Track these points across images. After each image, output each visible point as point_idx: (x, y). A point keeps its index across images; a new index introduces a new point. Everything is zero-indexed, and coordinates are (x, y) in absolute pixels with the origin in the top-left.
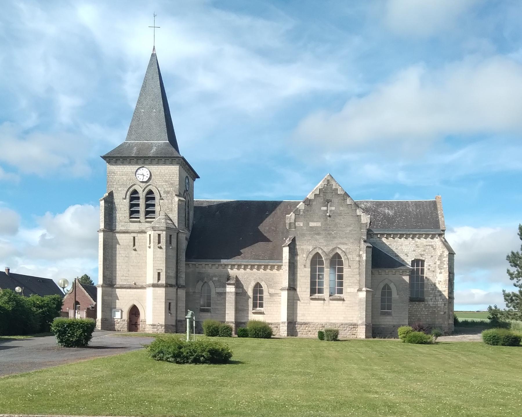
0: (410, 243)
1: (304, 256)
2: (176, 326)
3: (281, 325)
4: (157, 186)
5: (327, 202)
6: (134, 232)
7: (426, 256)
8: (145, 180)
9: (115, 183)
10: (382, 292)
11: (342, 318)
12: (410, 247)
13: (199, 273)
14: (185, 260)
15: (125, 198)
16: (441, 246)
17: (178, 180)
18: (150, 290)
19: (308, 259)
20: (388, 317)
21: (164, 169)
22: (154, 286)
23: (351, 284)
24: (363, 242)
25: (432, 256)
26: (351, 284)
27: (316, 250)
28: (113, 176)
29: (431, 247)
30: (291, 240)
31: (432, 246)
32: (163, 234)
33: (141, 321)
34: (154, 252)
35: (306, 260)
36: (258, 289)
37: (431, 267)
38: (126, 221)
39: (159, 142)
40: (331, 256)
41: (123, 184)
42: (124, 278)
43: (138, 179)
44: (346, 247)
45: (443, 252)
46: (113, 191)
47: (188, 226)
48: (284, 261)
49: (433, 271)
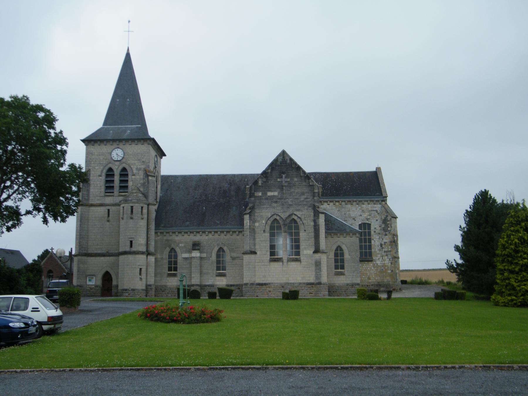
1: (264, 222)
3: (244, 287)
8: (119, 159)
9: (93, 163)
10: (335, 253)
11: (300, 279)
12: (357, 212)
14: (154, 229)
15: (100, 176)
19: (266, 225)
20: (342, 277)
21: (136, 149)
23: (307, 247)
26: (307, 247)
29: (375, 212)
39: (132, 126)
42: (99, 247)
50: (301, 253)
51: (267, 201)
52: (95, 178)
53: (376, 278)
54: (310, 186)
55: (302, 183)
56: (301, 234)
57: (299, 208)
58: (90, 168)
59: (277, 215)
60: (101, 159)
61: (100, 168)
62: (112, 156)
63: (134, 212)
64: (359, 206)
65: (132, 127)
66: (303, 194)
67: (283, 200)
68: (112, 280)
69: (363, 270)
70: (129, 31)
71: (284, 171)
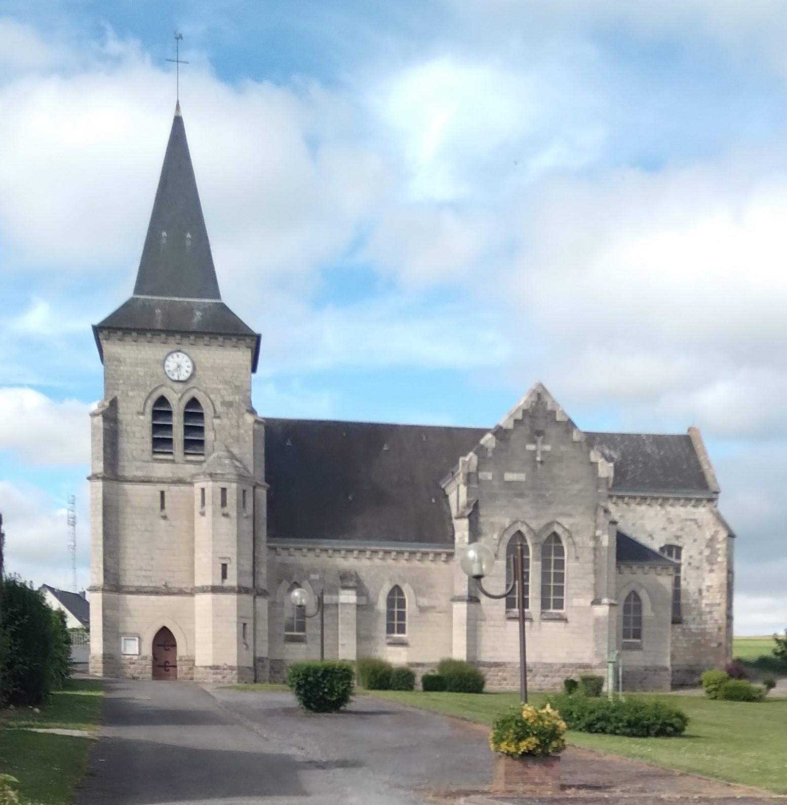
1: (496, 536)
2: (255, 669)
5: (537, 434)
6: (163, 482)
13: (283, 565)
15: (143, 414)
18: (204, 601)
19: (502, 542)
22: (215, 590)
23: (579, 591)
25: (695, 540)
26: (579, 591)
27: (516, 525)
28: (116, 366)
30: (472, 505)
31: (695, 521)
32: (233, 489)
33: (181, 660)
34: (214, 524)
35: (498, 545)
36: (396, 597)
40: (545, 536)
41: (138, 385)
42: (143, 573)
45: (716, 532)
46: (118, 397)
48: (457, 546)
49: (698, 568)
58: (116, 394)
60: (142, 374)
63: (228, 502)
65: (204, 303)
68: (175, 645)
70: (177, 61)
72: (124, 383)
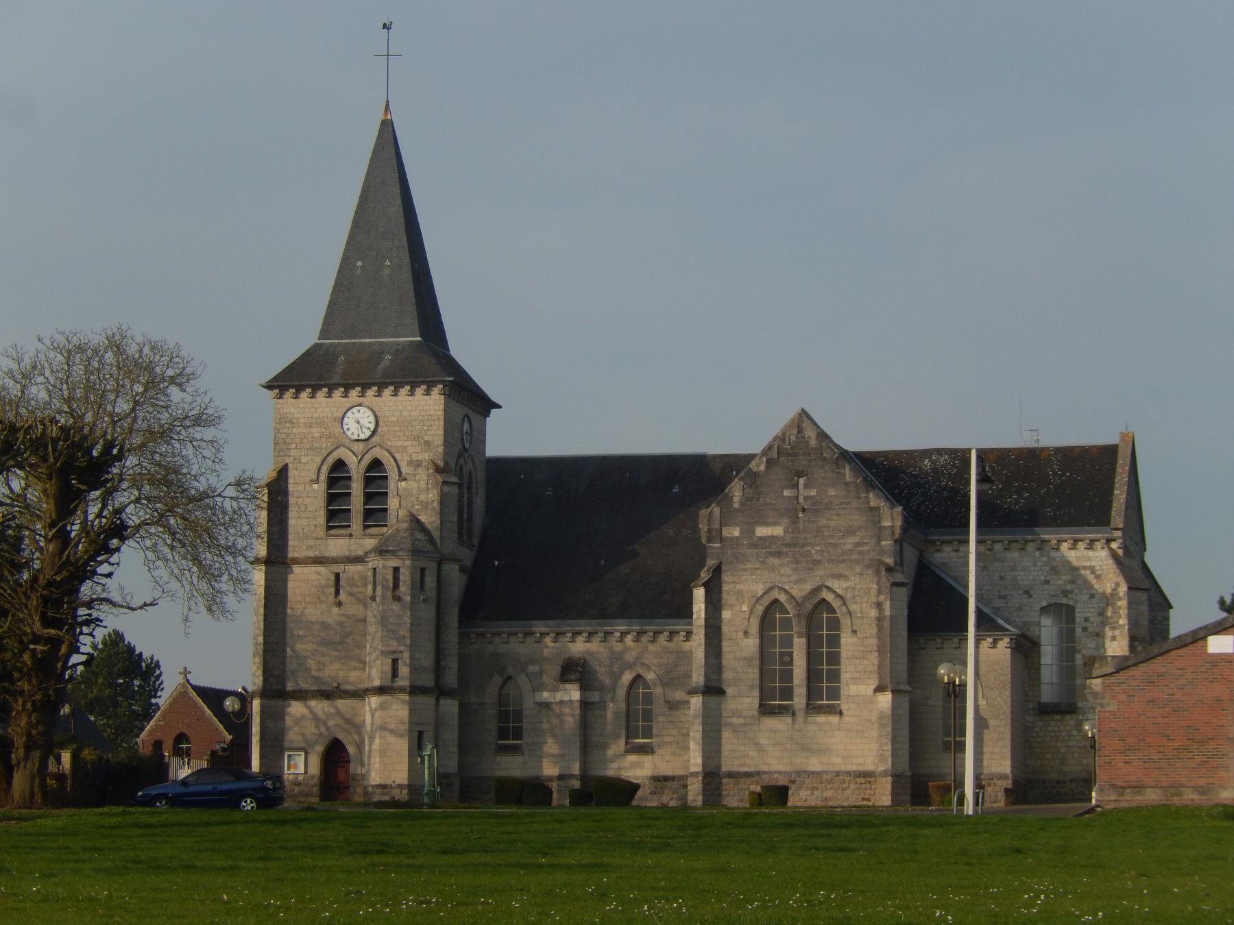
0: (1035, 563)
1: (745, 608)
4: (393, 451)
7: (1076, 595)
8: (362, 437)
9: (294, 446)
12: (1035, 573)
15: (317, 481)
16: (1112, 571)
17: (443, 433)
19: (752, 616)
23: (857, 675)
24: (884, 573)
26: (857, 675)
30: (711, 570)
35: (749, 619)
37: (1092, 623)
38: (319, 536)
39: (397, 339)
40: (809, 606)
43: (349, 434)
44: (844, 584)
45: (1117, 584)
46: (290, 465)
47: (470, 537)
49: (1097, 635)
50: (842, 692)
51: (754, 551)
52: (301, 488)
53: (1085, 761)
54: (872, 509)
55: (849, 503)
56: (843, 641)
57: (840, 569)
59: (781, 589)
60: (317, 435)
61: (313, 460)
62: (345, 427)
64: (1042, 556)
65: (398, 344)
66: (850, 532)
67: (796, 550)
69: (1048, 739)
71: (801, 468)
72: (296, 448)
